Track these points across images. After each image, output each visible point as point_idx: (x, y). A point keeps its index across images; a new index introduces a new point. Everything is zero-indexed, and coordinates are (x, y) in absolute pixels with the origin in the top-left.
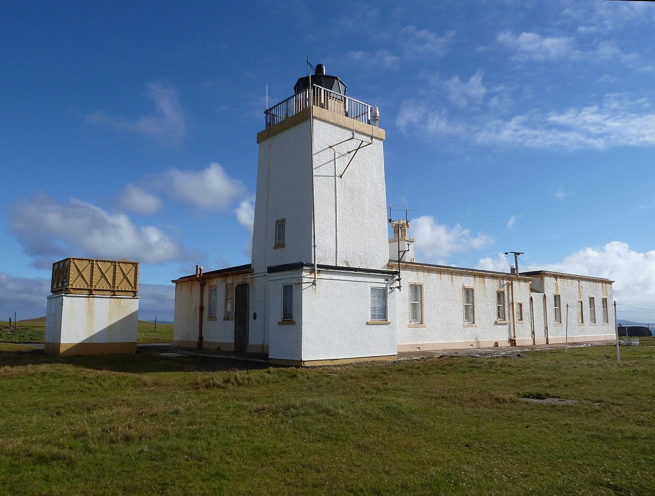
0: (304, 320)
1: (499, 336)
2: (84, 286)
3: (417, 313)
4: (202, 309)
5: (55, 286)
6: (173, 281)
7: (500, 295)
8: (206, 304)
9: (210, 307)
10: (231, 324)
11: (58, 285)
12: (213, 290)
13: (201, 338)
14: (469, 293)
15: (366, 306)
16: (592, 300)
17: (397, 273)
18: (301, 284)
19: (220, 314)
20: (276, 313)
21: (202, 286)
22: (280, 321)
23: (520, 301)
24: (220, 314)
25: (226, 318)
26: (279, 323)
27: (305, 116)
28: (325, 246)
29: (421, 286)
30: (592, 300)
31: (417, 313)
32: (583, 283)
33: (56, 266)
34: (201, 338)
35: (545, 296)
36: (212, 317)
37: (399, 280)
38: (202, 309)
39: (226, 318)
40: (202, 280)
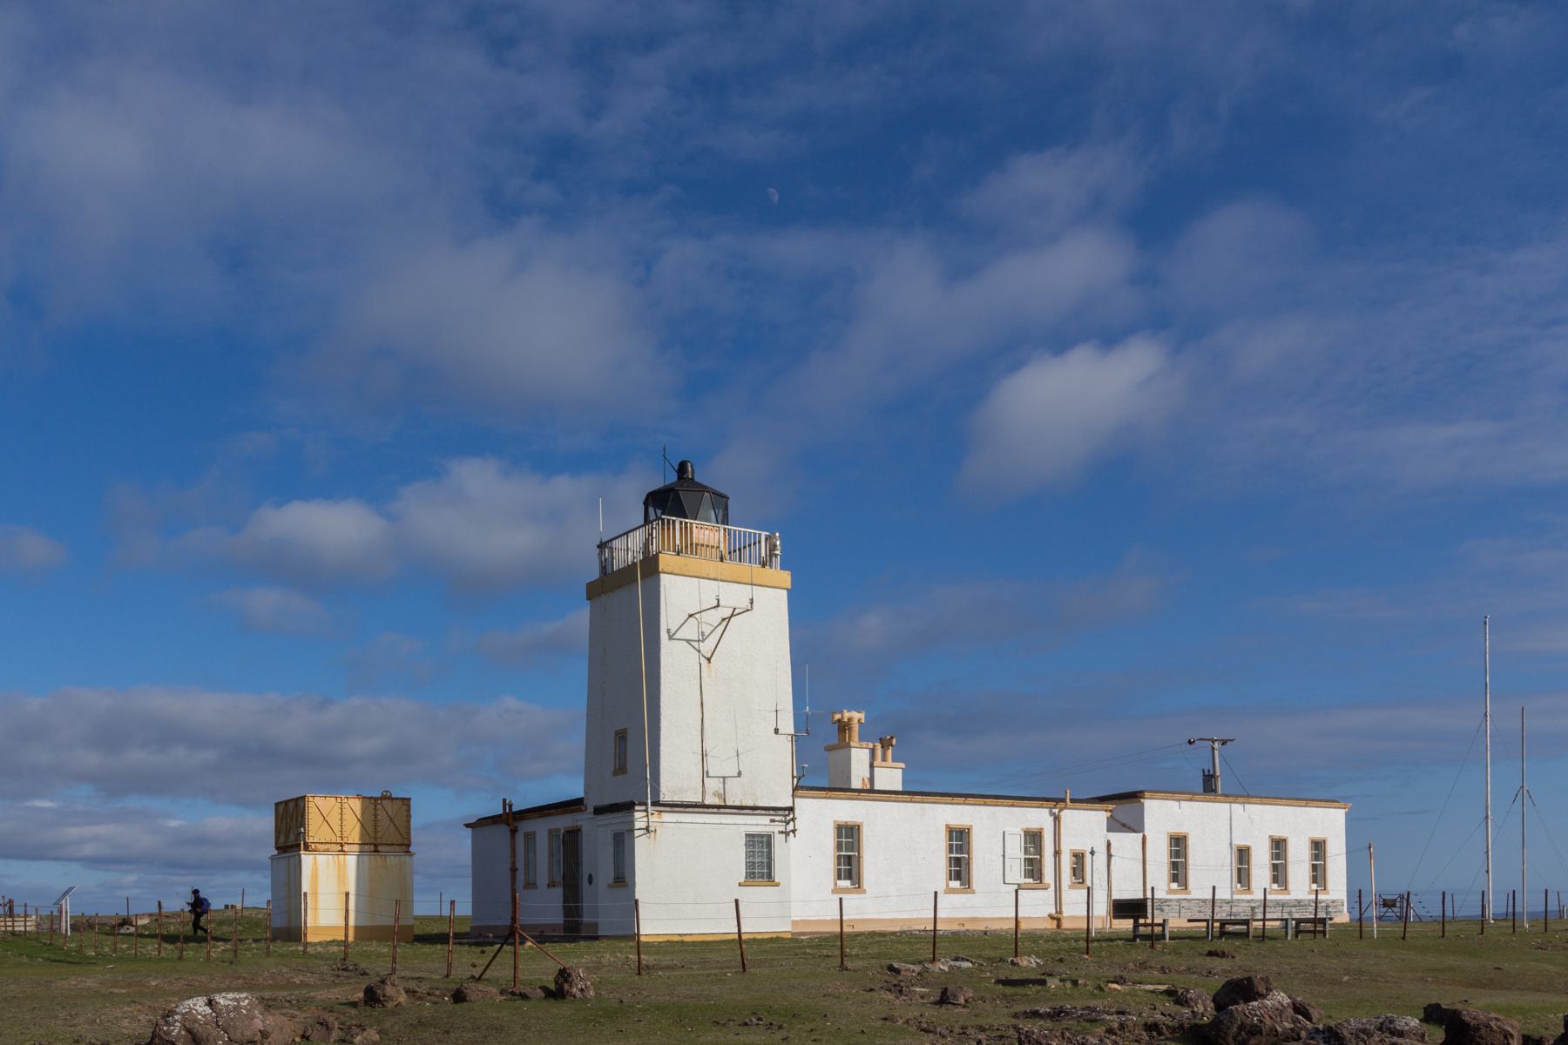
0: (637, 880)
1: (1036, 908)
2: (330, 837)
3: (849, 867)
4: (514, 870)
5: (282, 839)
6: (467, 826)
7: (1033, 838)
8: (520, 865)
9: (527, 865)
10: (559, 891)
11: (287, 837)
12: (530, 837)
13: (514, 919)
14: (959, 838)
15: (737, 860)
16: (1279, 846)
17: (791, 809)
18: (632, 831)
19: (542, 878)
20: (605, 874)
21: (514, 832)
22: (742, 880)
23: (1078, 847)
24: (542, 878)
25: (551, 885)
26: (609, 886)
27: (650, 567)
28: (677, 772)
29: (1285, 840)
30: (1279, 846)
31: (849, 867)
32: (697, 799)
33: (281, 808)
34: (514, 919)
35: (1144, 838)
36: (531, 885)
37: (793, 819)
38: (514, 870)
39: (551, 885)
40: (511, 819)
